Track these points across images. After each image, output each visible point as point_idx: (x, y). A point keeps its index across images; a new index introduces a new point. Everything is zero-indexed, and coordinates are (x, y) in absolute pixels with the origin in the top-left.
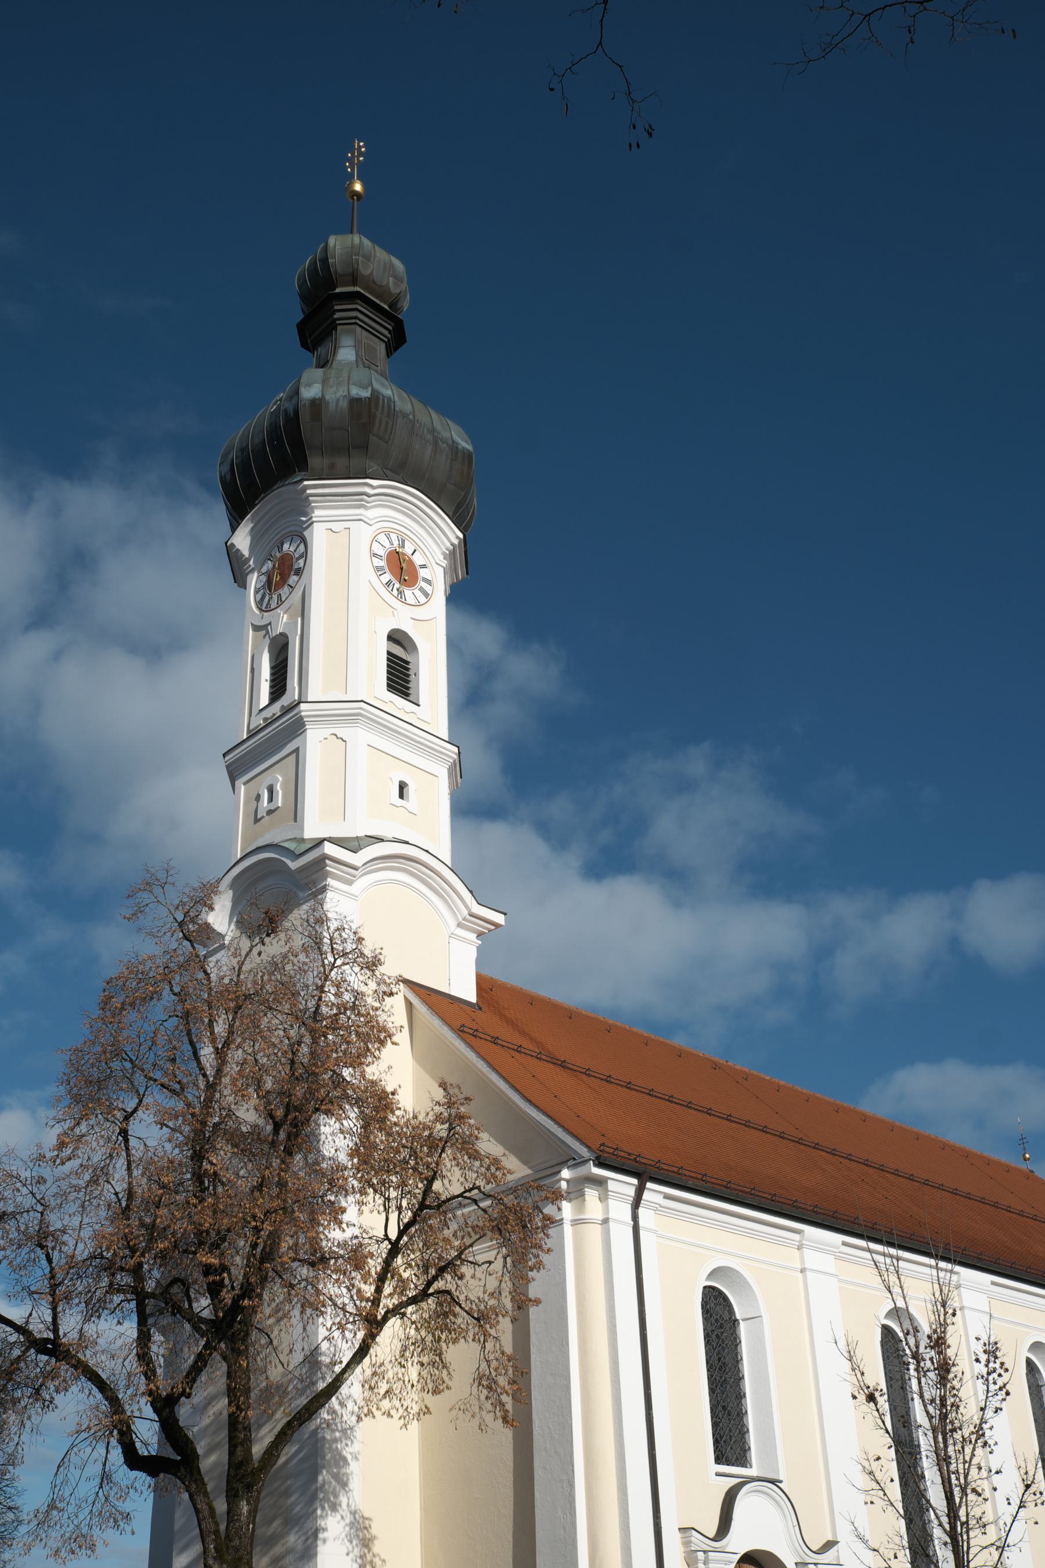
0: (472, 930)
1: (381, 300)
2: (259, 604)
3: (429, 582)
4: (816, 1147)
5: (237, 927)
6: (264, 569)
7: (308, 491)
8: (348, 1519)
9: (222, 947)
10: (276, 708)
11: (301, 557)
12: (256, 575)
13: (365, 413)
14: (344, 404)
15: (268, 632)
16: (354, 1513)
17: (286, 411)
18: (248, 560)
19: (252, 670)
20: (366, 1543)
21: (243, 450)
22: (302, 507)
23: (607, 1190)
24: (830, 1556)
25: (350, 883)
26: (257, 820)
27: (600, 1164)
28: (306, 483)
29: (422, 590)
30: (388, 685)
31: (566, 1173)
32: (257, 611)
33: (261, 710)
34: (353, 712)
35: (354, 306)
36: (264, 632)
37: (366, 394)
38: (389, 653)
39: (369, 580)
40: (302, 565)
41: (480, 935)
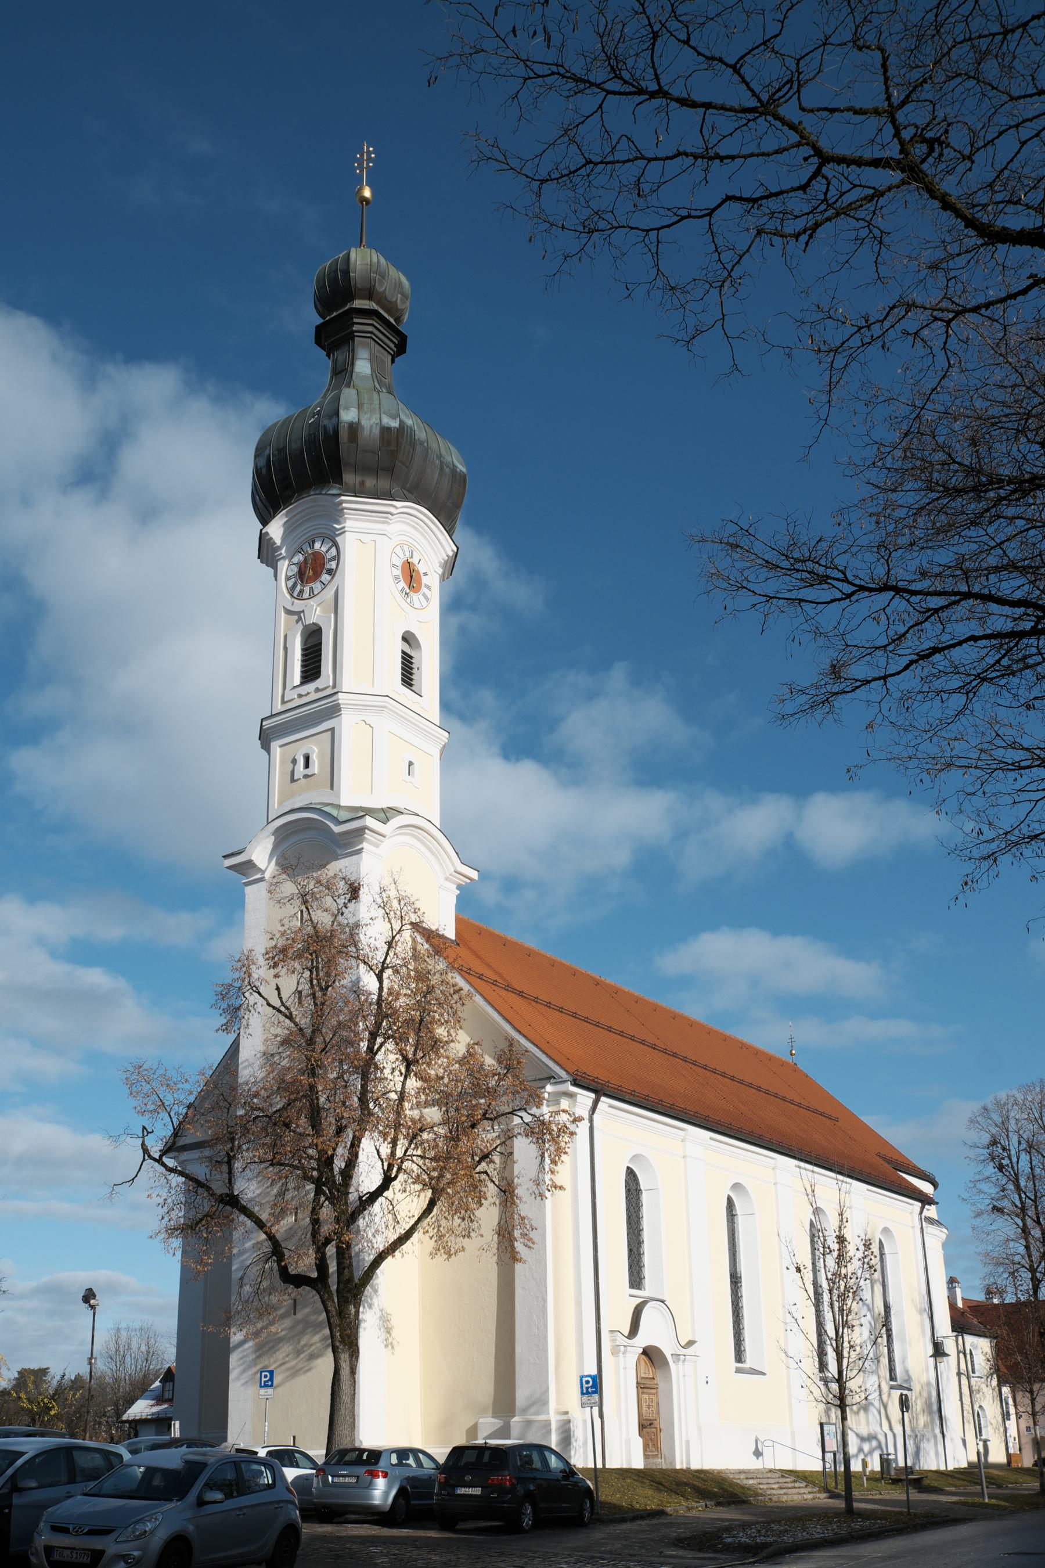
0: (454, 883)
1: (389, 314)
2: (291, 590)
3: (429, 588)
4: (674, 1055)
5: (277, 864)
6: (295, 560)
7: (344, 505)
8: (379, 1314)
9: (262, 880)
10: (311, 687)
11: (333, 559)
12: (287, 562)
13: (394, 441)
14: (376, 431)
15: (300, 619)
16: (382, 1311)
17: (325, 427)
18: (279, 548)
19: (286, 648)
20: (388, 1331)
21: (281, 450)
22: (337, 514)
23: (575, 1101)
24: (689, 1351)
25: (377, 846)
26: (293, 780)
27: (575, 1084)
28: (343, 498)
29: (424, 595)
30: (403, 680)
31: (549, 1088)
32: (288, 596)
33: (295, 687)
34: (380, 701)
35: (370, 322)
36: (296, 617)
37: (395, 424)
38: (403, 652)
39: (392, 586)
40: (334, 567)
41: (459, 887)
